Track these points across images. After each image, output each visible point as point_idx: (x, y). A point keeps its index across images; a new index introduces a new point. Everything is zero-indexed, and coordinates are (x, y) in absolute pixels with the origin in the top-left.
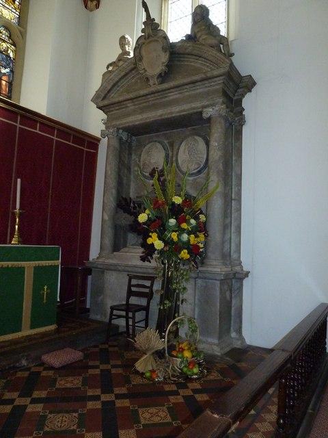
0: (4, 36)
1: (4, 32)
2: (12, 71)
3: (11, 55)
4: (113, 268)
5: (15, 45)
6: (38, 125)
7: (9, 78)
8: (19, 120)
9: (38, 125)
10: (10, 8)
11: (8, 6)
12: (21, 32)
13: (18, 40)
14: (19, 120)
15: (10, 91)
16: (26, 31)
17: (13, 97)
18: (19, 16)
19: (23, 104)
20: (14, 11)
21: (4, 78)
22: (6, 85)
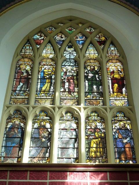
0: (120, 118)
1: (120, 115)
2: (132, 138)
3: (128, 128)
4: (78, 151)
5: (129, 119)
6: (128, 174)
7: (130, 144)
8: (128, 177)
9: (128, 174)
10: (120, 99)
11: (119, 98)
12: (130, 109)
13: (131, 115)
14: (128, 177)
15: (134, 153)
16: (134, 107)
17: (108, 162)
18: (128, 101)
19: (23, 163)
20: (123, 98)
21: (127, 146)
22: (129, 150)
